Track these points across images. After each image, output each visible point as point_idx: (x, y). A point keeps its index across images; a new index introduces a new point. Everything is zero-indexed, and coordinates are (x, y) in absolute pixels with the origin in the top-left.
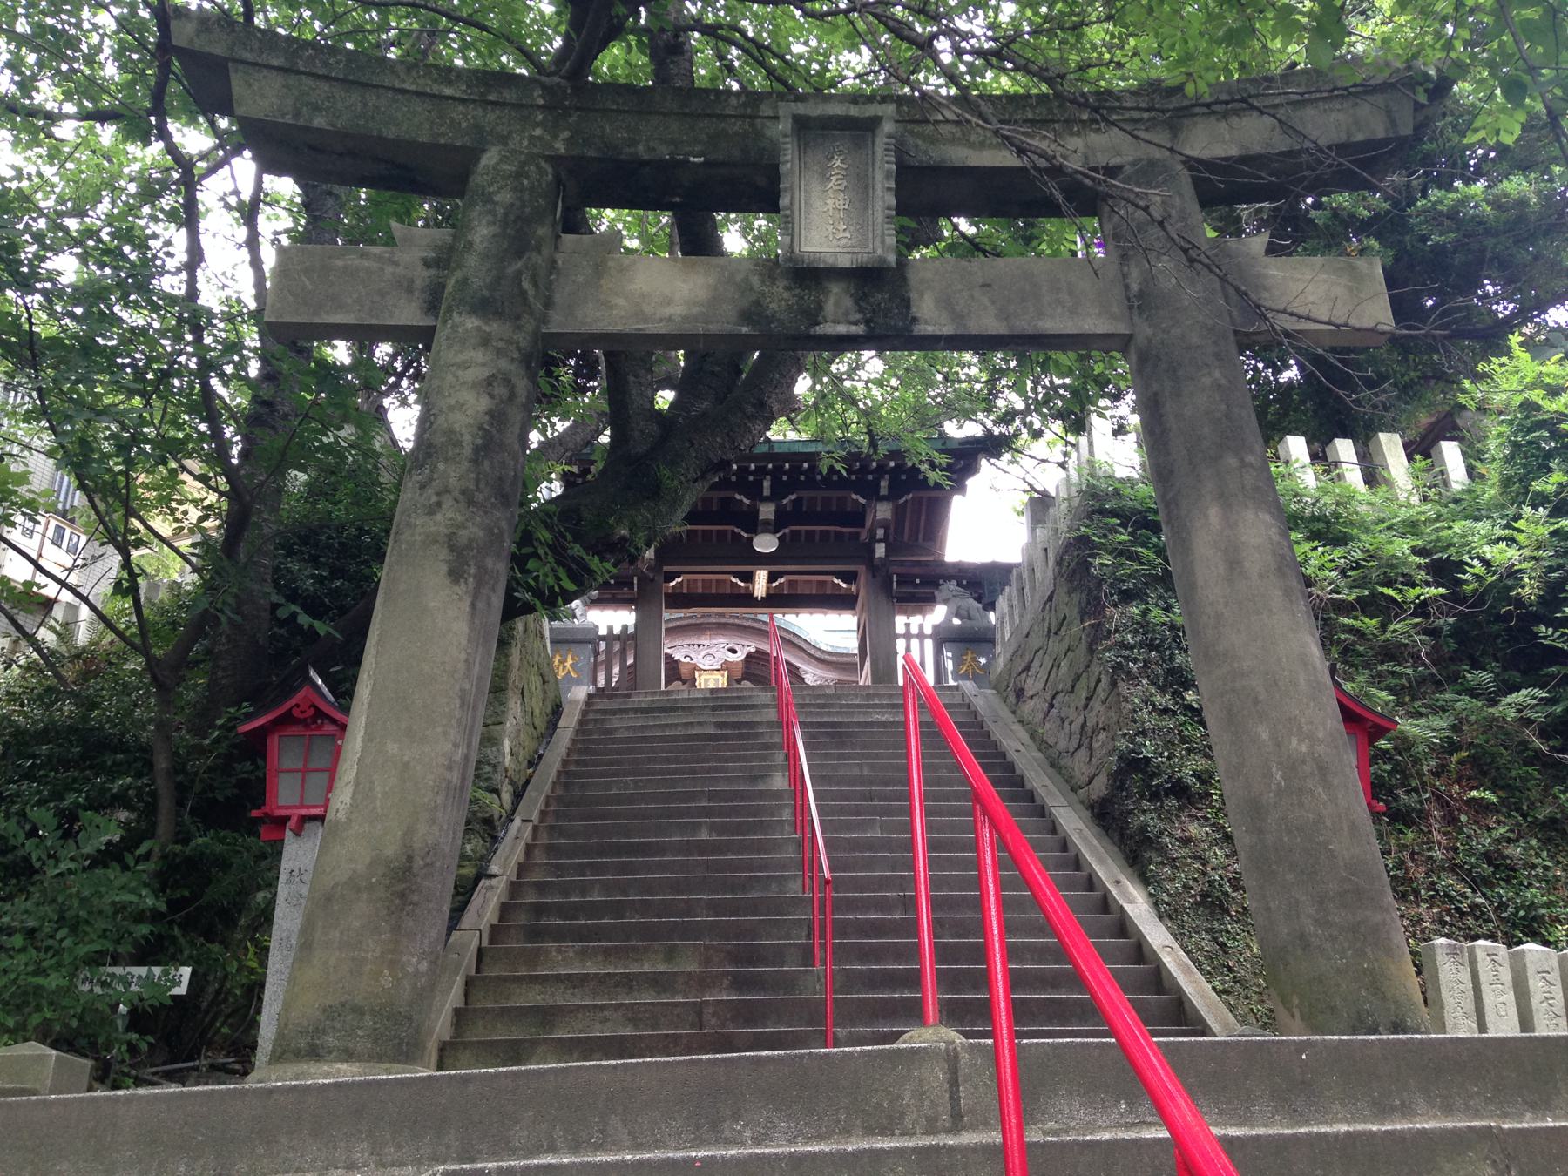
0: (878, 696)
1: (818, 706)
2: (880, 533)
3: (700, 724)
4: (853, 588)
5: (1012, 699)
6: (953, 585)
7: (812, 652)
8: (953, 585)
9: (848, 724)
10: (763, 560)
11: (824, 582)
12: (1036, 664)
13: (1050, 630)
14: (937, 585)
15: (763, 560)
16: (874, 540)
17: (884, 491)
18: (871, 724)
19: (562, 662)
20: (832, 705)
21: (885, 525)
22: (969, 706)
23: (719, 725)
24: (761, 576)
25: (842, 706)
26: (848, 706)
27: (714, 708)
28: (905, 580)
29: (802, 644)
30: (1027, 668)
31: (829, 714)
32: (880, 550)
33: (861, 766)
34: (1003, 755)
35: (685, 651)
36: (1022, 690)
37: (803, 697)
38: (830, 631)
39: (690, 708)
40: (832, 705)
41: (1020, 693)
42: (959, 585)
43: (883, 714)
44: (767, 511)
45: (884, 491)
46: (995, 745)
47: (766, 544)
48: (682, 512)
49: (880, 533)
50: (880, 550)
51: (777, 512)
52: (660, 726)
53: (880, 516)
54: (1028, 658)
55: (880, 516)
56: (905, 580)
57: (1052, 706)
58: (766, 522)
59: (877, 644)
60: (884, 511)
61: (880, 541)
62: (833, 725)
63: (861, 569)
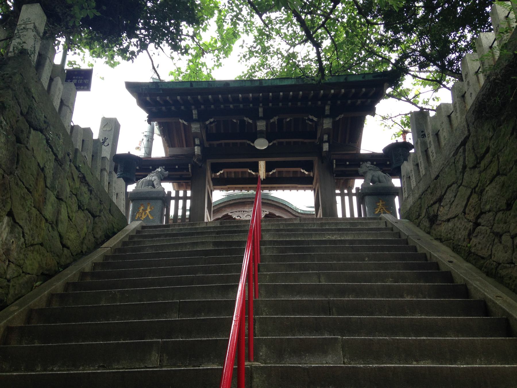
0: (329, 224)
1: (288, 230)
2: (326, 137)
3: (203, 243)
4: (312, 174)
5: (427, 224)
6: (368, 164)
7: (294, 213)
8: (368, 164)
9: (308, 242)
10: (262, 154)
11: (297, 172)
12: (449, 195)
13: (464, 167)
14: (359, 166)
15: (262, 154)
16: (322, 142)
17: (327, 112)
18: (325, 242)
19: (144, 210)
20: (297, 230)
21: (327, 132)
22: (392, 229)
23: (215, 244)
24: (262, 165)
25: (304, 230)
26: (309, 230)
27: (218, 233)
28: (341, 162)
29: (289, 210)
30: (440, 200)
31: (295, 235)
32: (326, 147)
33: (319, 276)
34: (436, 265)
35: (238, 214)
36: (436, 216)
37: (278, 225)
38: (301, 200)
39: (202, 233)
40: (297, 230)
41: (433, 220)
42: (372, 164)
43: (333, 235)
44: (261, 125)
45: (327, 112)
46: (424, 256)
47: (261, 144)
48: (161, 63)
49: (326, 137)
50: (326, 147)
51: (267, 126)
52: (174, 245)
53: (325, 126)
54: (438, 194)
55: (325, 126)
56: (341, 162)
57: (477, 224)
58: (261, 132)
59: (325, 204)
60: (327, 124)
61: (326, 142)
62: (297, 242)
63: (315, 159)
